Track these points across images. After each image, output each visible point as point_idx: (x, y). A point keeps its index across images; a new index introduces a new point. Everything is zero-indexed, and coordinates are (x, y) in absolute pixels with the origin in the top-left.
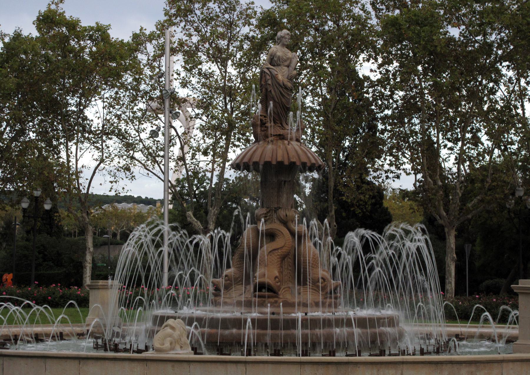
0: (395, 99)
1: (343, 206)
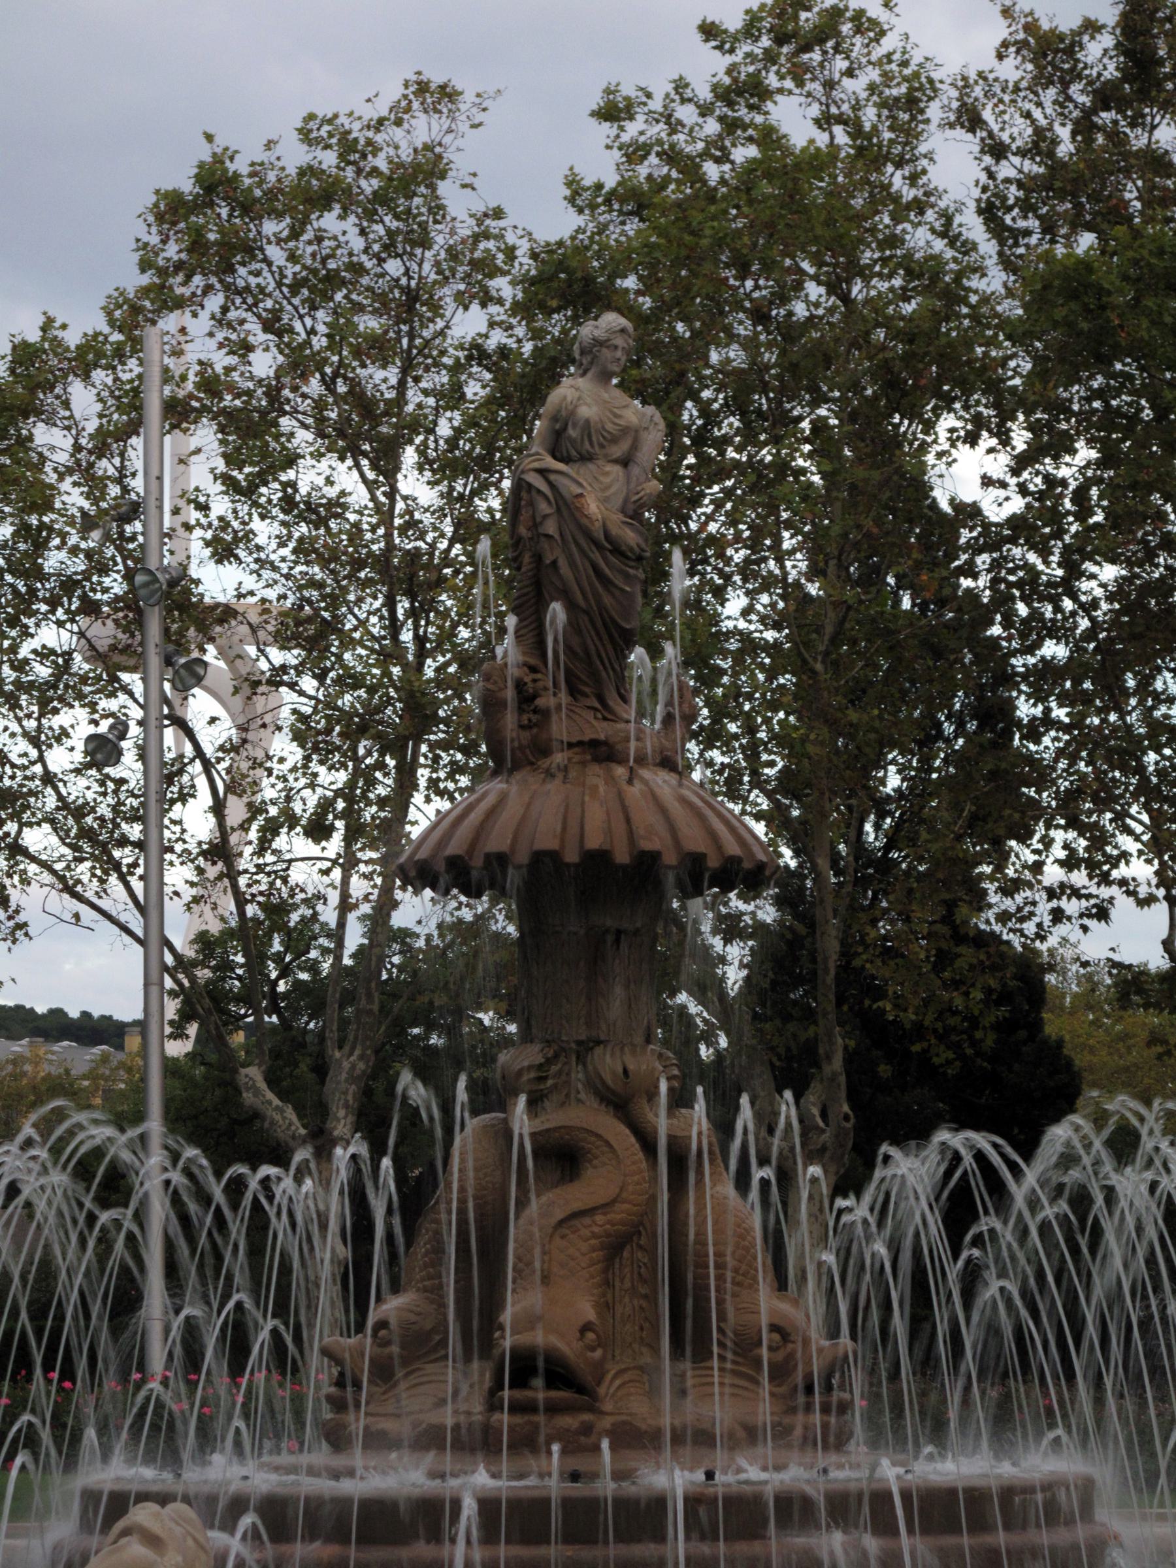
0: (1083, 598)
1: (877, 1035)
